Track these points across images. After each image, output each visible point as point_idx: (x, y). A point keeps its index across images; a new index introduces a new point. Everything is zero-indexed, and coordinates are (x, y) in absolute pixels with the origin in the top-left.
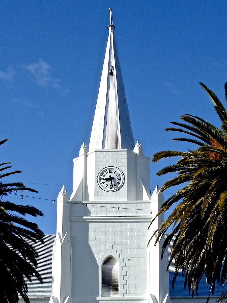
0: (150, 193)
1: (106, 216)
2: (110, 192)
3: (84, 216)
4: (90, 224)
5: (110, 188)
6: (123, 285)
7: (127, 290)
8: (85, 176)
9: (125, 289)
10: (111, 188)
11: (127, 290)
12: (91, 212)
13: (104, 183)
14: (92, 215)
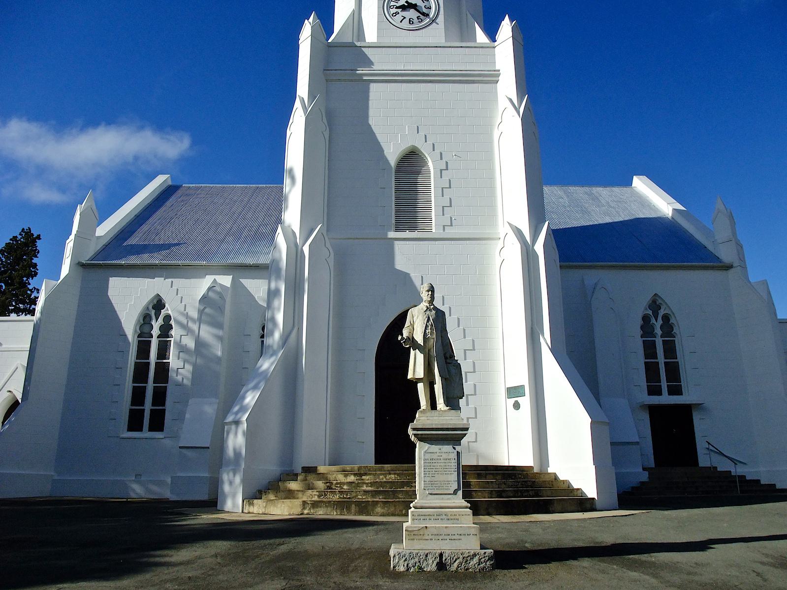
0: (492, 32)
1: (402, 68)
2: (409, 31)
3: (358, 69)
4: (373, 86)
5: (410, 24)
6: (443, 207)
7: (451, 218)
8: (357, 8)
9: (447, 216)
10: (411, 22)
11: (451, 218)
12: (375, 64)
13: (397, 13)
14: (375, 67)
